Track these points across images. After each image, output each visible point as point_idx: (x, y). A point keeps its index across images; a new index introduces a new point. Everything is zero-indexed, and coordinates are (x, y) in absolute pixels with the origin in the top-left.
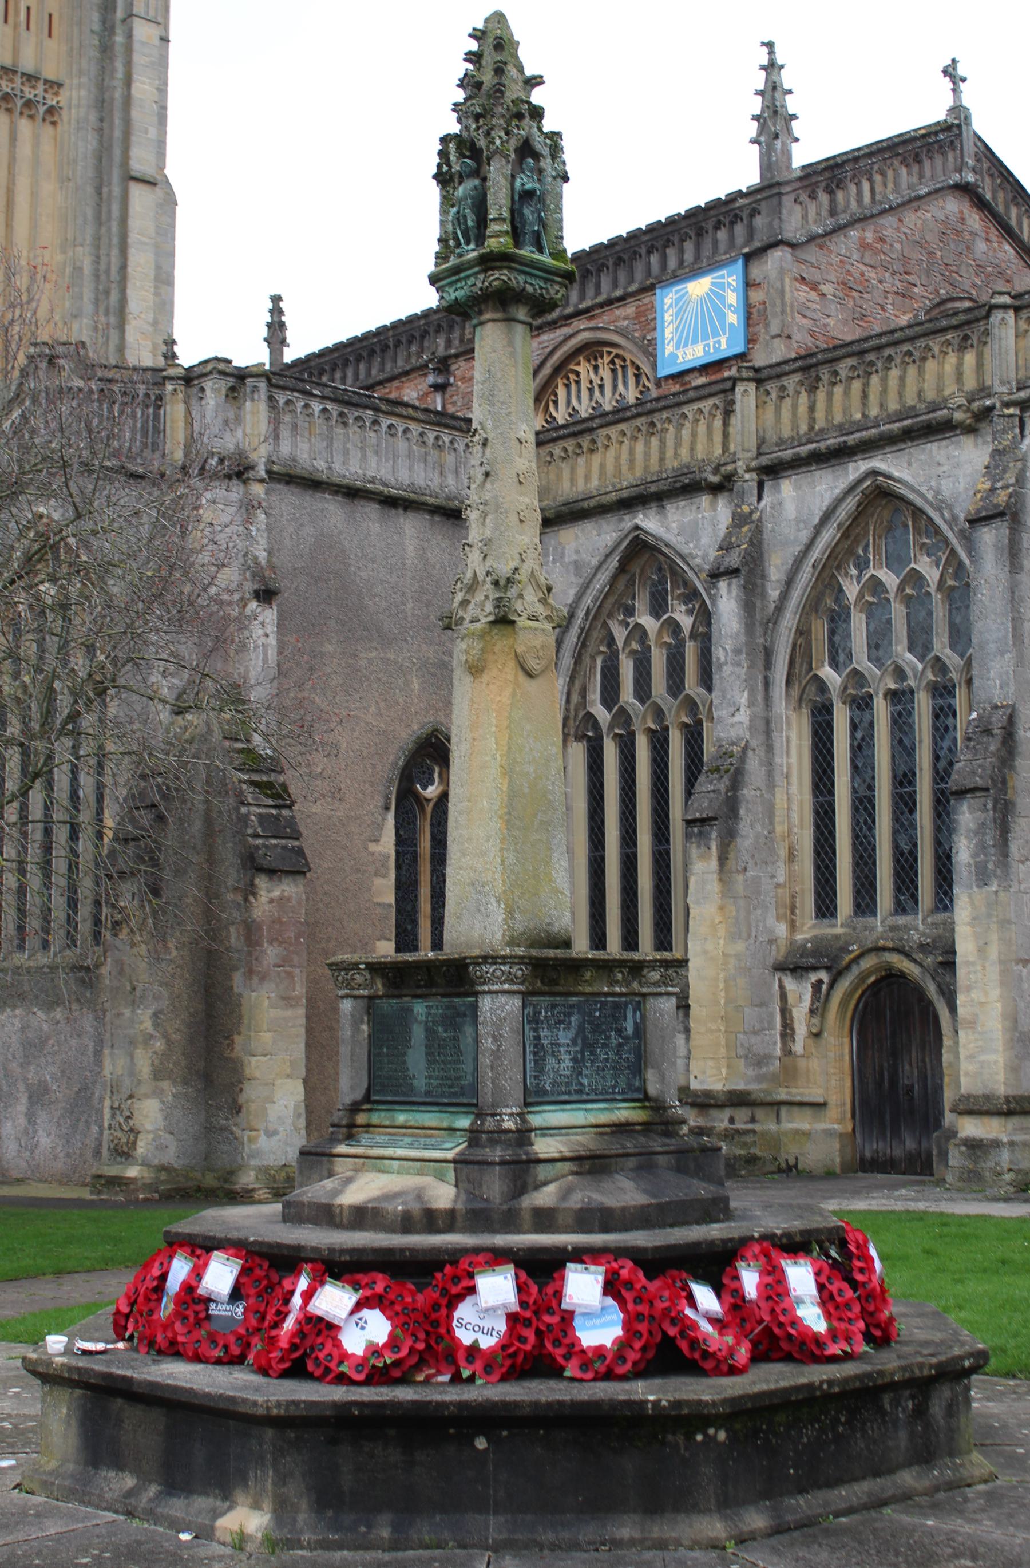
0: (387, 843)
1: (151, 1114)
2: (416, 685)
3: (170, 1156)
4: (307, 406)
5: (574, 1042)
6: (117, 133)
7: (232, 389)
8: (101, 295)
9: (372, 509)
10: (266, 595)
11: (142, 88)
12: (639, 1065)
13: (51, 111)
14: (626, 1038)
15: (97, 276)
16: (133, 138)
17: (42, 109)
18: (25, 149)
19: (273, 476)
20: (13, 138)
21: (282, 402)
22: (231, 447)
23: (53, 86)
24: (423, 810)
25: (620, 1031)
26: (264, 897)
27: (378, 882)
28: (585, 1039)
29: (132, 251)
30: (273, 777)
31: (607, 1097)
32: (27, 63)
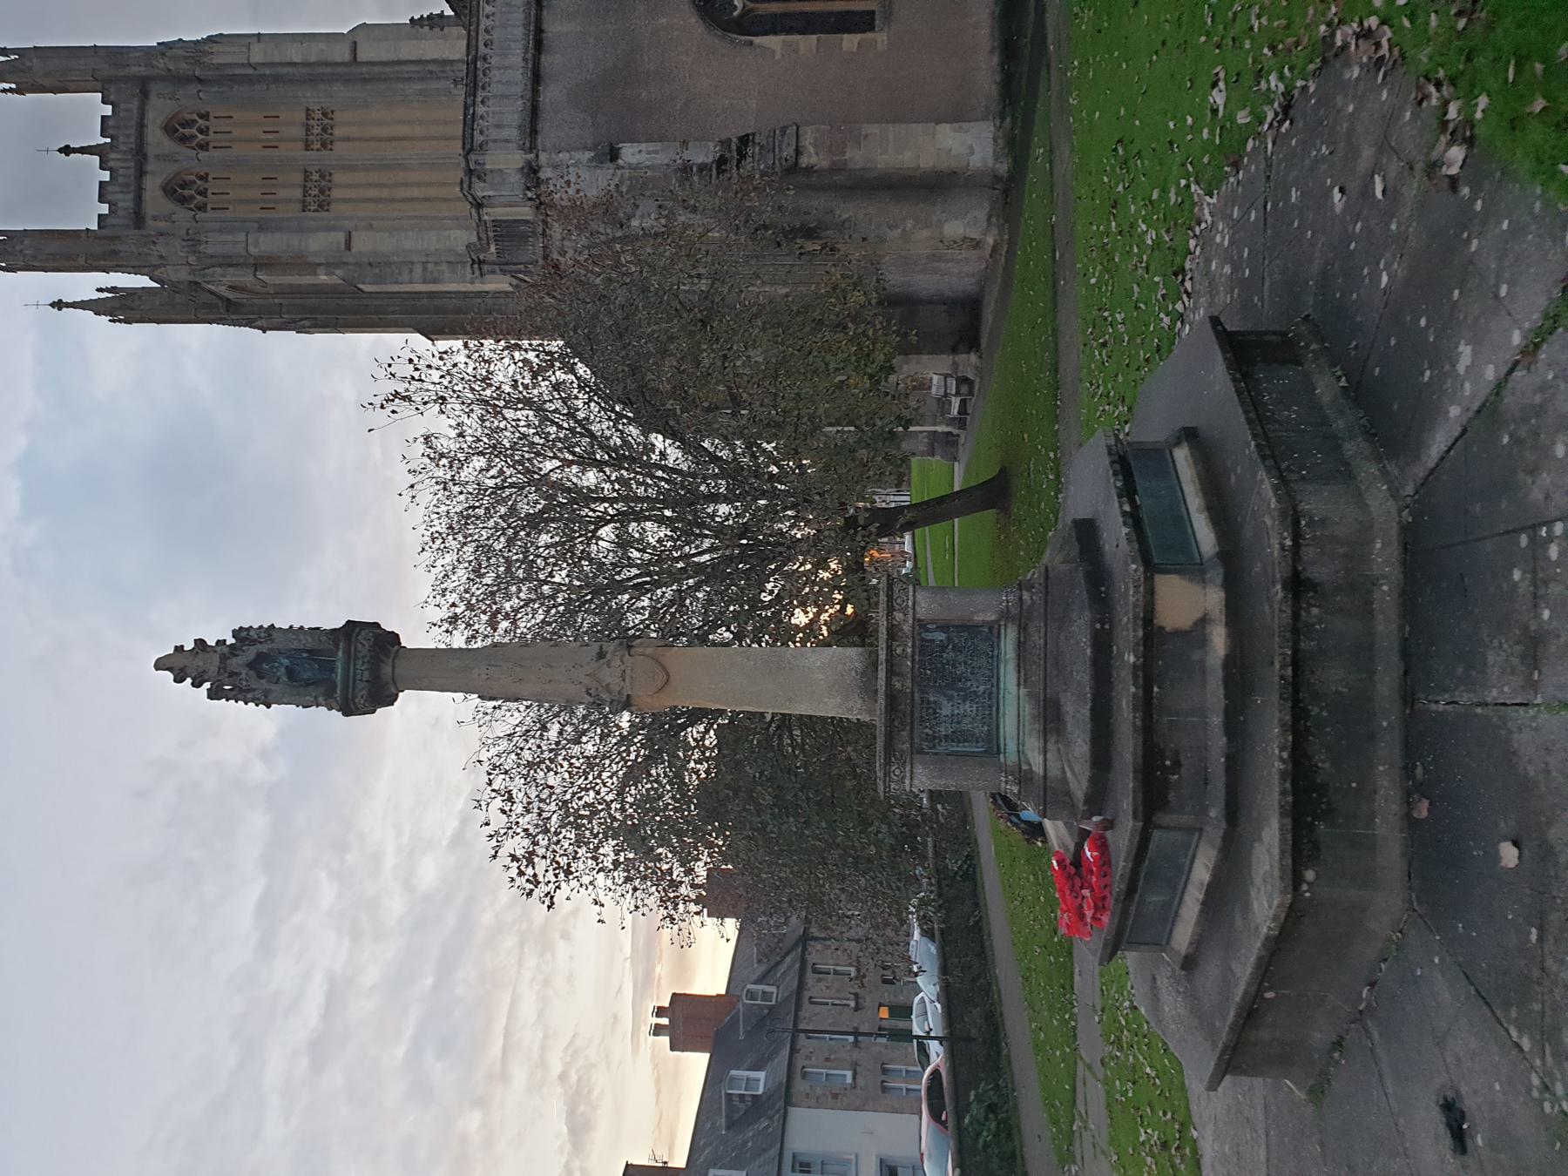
0: (773, 42)
1: (954, 229)
2: (664, 21)
3: (982, 215)
5: (950, 698)
6: (329, 70)
8: (433, 76)
9: (546, 60)
10: (614, 154)
11: (295, 54)
12: (971, 629)
13: (325, 114)
14: (949, 639)
15: (423, 79)
16: (329, 59)
17: (326, 121)
20: (348, 139)
23: (309, 113)
24: (751, 10)
25: (943, 648)
26: (814, 160)
27: (802, 47)
29: (401, 57)
30: (734, 147)
31: (994, 660)
32: (300, 132)
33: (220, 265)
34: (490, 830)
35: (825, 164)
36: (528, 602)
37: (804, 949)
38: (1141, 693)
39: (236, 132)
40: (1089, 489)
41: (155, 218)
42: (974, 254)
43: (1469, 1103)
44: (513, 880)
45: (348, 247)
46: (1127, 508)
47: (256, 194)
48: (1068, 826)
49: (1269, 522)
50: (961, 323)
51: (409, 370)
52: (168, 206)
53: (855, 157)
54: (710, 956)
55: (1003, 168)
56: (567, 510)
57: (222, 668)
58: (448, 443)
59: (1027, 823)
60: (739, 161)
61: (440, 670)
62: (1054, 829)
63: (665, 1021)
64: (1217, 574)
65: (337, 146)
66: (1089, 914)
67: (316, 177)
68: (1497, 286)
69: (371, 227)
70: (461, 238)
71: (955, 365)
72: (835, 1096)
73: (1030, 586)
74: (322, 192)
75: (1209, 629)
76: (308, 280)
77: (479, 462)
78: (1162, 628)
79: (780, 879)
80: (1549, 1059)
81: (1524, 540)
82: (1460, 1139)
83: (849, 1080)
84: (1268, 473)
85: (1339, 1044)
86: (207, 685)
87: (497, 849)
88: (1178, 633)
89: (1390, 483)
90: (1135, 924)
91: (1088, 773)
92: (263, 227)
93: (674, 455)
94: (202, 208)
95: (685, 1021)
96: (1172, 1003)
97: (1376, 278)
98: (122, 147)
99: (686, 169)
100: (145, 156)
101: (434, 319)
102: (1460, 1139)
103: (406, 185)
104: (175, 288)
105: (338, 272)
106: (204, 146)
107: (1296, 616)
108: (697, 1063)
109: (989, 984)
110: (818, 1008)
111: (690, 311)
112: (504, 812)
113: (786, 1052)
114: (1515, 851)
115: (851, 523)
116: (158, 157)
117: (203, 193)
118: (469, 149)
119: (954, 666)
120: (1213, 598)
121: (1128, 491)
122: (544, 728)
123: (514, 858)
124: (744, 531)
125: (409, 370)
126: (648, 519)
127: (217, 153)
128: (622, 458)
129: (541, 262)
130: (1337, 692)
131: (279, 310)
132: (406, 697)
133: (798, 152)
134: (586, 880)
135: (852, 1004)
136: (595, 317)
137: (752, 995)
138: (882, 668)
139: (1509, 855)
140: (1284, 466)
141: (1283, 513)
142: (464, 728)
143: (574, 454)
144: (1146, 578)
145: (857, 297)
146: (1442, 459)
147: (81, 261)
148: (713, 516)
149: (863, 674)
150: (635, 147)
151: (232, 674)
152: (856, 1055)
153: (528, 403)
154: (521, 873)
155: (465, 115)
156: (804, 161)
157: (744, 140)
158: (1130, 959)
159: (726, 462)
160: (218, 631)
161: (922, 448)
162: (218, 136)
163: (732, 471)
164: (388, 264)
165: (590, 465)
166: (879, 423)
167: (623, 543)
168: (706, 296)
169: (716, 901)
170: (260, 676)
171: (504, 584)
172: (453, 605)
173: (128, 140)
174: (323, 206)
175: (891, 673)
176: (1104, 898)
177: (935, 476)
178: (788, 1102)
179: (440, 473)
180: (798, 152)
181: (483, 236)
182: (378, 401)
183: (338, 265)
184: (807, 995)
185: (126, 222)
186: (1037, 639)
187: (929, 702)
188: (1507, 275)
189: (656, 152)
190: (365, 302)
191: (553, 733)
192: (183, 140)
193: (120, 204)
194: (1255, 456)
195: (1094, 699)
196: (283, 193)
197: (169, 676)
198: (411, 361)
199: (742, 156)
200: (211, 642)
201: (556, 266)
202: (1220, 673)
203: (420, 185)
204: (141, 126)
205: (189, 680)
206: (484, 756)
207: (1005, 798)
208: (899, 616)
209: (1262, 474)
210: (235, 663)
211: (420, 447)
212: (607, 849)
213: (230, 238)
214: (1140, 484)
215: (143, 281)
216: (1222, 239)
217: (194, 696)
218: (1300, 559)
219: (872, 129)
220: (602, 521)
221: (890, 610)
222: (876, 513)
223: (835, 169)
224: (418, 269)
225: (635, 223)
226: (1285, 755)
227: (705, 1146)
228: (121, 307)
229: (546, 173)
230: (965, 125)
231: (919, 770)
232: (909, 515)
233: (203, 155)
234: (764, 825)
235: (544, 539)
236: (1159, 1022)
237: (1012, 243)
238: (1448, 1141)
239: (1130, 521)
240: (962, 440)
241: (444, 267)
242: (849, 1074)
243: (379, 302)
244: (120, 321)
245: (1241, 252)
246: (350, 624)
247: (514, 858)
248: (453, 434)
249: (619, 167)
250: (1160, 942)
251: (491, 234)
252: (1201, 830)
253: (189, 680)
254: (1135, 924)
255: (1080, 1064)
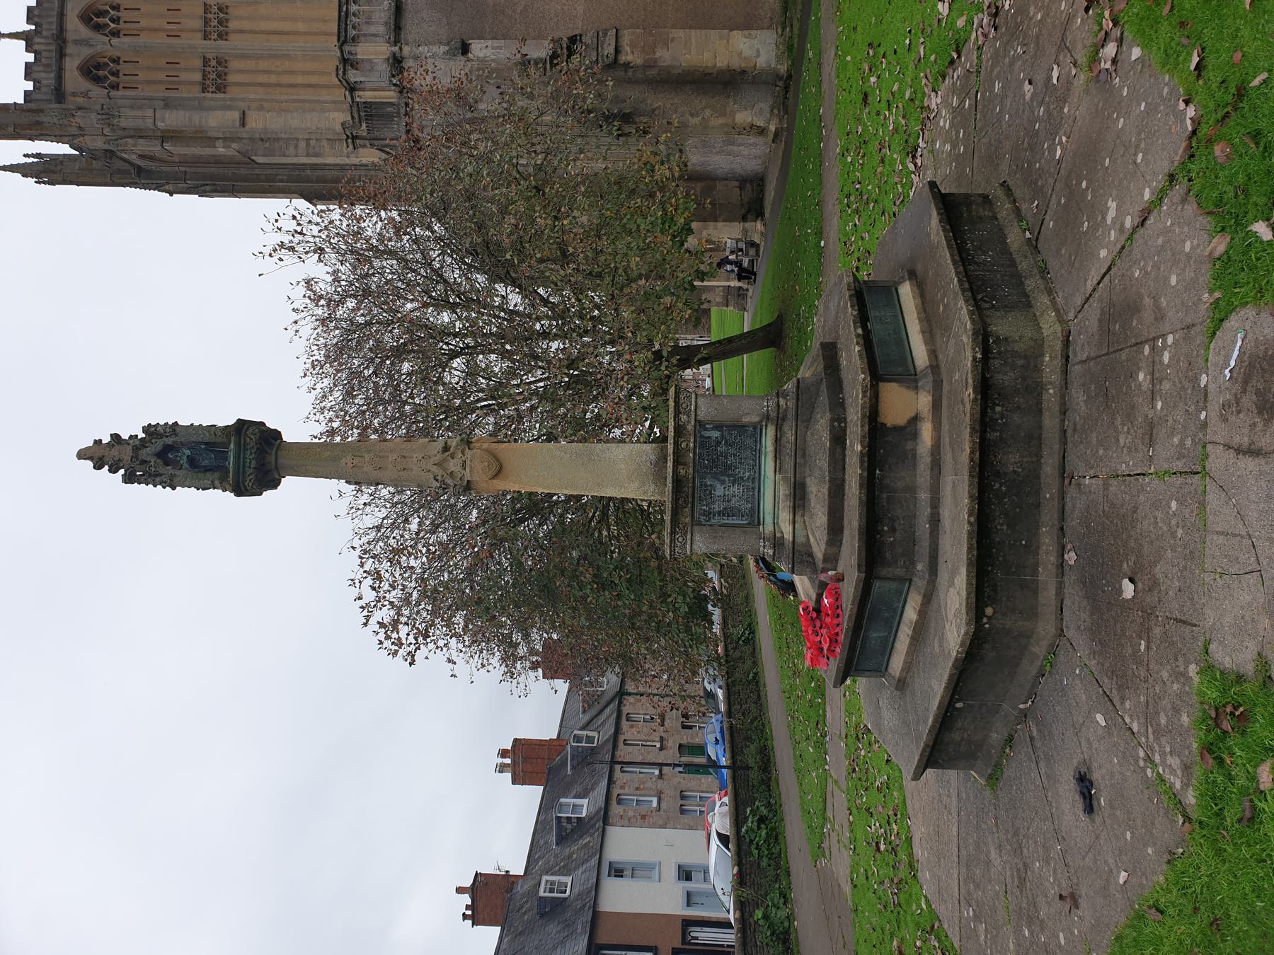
3: (765, 106)
4: (354, 14)
5: (723, 482)
7: (352, 66)
10: (465, 49)
12: (740, 428)
14: (722, 436)
17: (221, 15)
18: (245, 25)
19: (397, 41)
20: (241, 31)
21: (354, 32)
22: (385, 66)
26: (630, 58)
28: (723, 474)
31: (757, 454)
32: (199, 24)
33: (131, 137)
34: (362, 603)
35: (639, 62)
36: (393, 419)
37: (620, 703)
38: (865, 474)
39: (144, 23)
40: (831, 316)
41: (74, 94)
42: (760, 140)
43: (1096, 776)
44: (381, 643)
45: (243, 124)
46: (860, 331)
47: (161, 76)
48: (812, 580)
49: (965, 340)
50: (750, 199)
51: (292, 225)
52: (85, 85)
53: (665, 56)
54: (540, 707)
55: (783, 69)
56: (425, 345)
57: (135, 457)
58: (324, 287)
59: (782, 581)
60: (569, 57)
61: (314, 460)
62: (802, 583)
63: (508, 761)
64: (927, 383)
65: (232, 37)
66: (825, 647)
67: (213, 63)
68: (1136, 155)
69: (261, 108)
70: (338, 117)
71: (745, 231)
72: (643, 817)
73: (785, 395)
74: (219, 76)
75: (919, 425)
76: (208, 151)
77: (351, 303)
78: (884, 425)
79: (598, 641)
80: (1151, 736)
81: (1147, 349)
82: (1089, 806)
83: (655, 804)
84: (966, 301)
85: (1010, 740)
86: (122, 471)
87: (368, 618)
88: (897, 429)
89: (1057, 311)
90: (861, 653)
91: (825, 538)
92: (168, 104)
93: (515, 299)
94: (115, 87)
95: (524, 761)
96: (889, 717)
97: (1052, 150)
98: (44, 33)
99: (525, 63)
100: (65, 41)
101: (316, 186)
102: (1089, 806)
103: (292, 72)
104: (93, 155)
105: (234, 145)
106: (116, 34)
107: (983, 412)
108: (534, 793)
109: (763, 725)
110: (630, 749)
111: (525, 179)
112: (374, 589)
113: (604, 783)
114: (1131, 586)
115: (658, 355)
116: (76, 42)
117: (116, 74)
118: (344, 39)
119: (726, 458)
120: (924, 401)
121: (863, 319)
122: (406, 521)
123: (381, 625)
124: (572, 364)
125: (292, 225)
126: (493, 352)
127: (126, 40)
128: (467, 301)
129: (404, 137)
130: (1014, 472)
131: (184, 177)
132: (288, 482)
133: (617, 51)
134: (441, 643)
135: (658, 745)
136: (448, 183)
137: (578, 739)
138: (670, 459)
139: (1128, 590)
140: (980, 297)
141: (975, 333)
142: (340, 520)
143: (431, 297)
144: (872, 385)
145: (662, 172)
146: (1094, 290)
147: (11, 129)
148: (546, 351)
149: (656, 464)
150: (483, 43)
151: (144, 462)
152: (660, 784)
153: (392, 253)
154: (388, 637)
155: (340, 12)
156: (623, 58)
157: (573, 40)
158: (861, 684)
159: (557, 306)
160: (132, 428)
161: (718, 299)
162: (128, 25)
163: (560, 314)
164: (277, 140)
165: (444, 307)
166: (681, 275)
167: (472, 372)
168: (539, 168)
169: (551, 666)
170: (167, 464)
171: (375, 402)
172: (331, 420)
173: (50, 27)
174: (221, 89)
175: (677, 463)
176: (837, 634)
177: (727, 322)
178: (606, 820)
179: (320, 311)
180: (617, 51)
181: (356, 116)
182: (267, 251)
183: (233, 140)
184: (622, 738)
185: (48, 97)
186: (790, 436)
187: (706, 485)
188: (1143, 145)
189: (500, 48)
190: (257, 171)
191: (414, 526)
192: (98, 28)
193: (44, 82)
194: (957, 288)
195: (832, 481)
196: (185, 76)
197: (89, 464)
198: (294, 217)
199: (571, 53)
200: (125, 436)
201: (417, 141)
202: (928, 459)
203: (303, 73)
204: (62, 15)
205: (106, 467)
206: (357, 543)
207: (763, 559)
208: (684, 418)
209: (961, 303)
210: (145, 453)
211: (302, 289)
212: (459, 618)
213: (140, 113)
214: (873, 313)
215: (63, 149)
216: (945, 122)
217: (111, 481)
218: (988, 369)
219: (679, 34)
220: (454, 355)
221: (677, 413)
222: (676, 349)
223: (646, 67)
224: (302, 145)
225: (482, 106)
226: (972, 519)
227: (540, 858)
228: (46, 171)
229: (409, 63)
230: (753, 32)
231: (697, 537)
232: (704, 353)
233: (115, 41)
234: (584, 598)
235: (406, 367)
236: (880, 733)
237: (790, 129)
238: (1080, 805)
239: (862, 341)
240: (750, 293)
241: (325, 143)
242: (655, 800)
243: (269, 172)
244: (45, 183)
245: (958, 133)
246: (241, 422)
247: (381, 625)
248: (329, 279)
249: (469, 60)
250: (880, 670)
251: (363, 114)
252: (911, 580)
253: (106, 467)
254: (861, 653)
255: (830, 780)
